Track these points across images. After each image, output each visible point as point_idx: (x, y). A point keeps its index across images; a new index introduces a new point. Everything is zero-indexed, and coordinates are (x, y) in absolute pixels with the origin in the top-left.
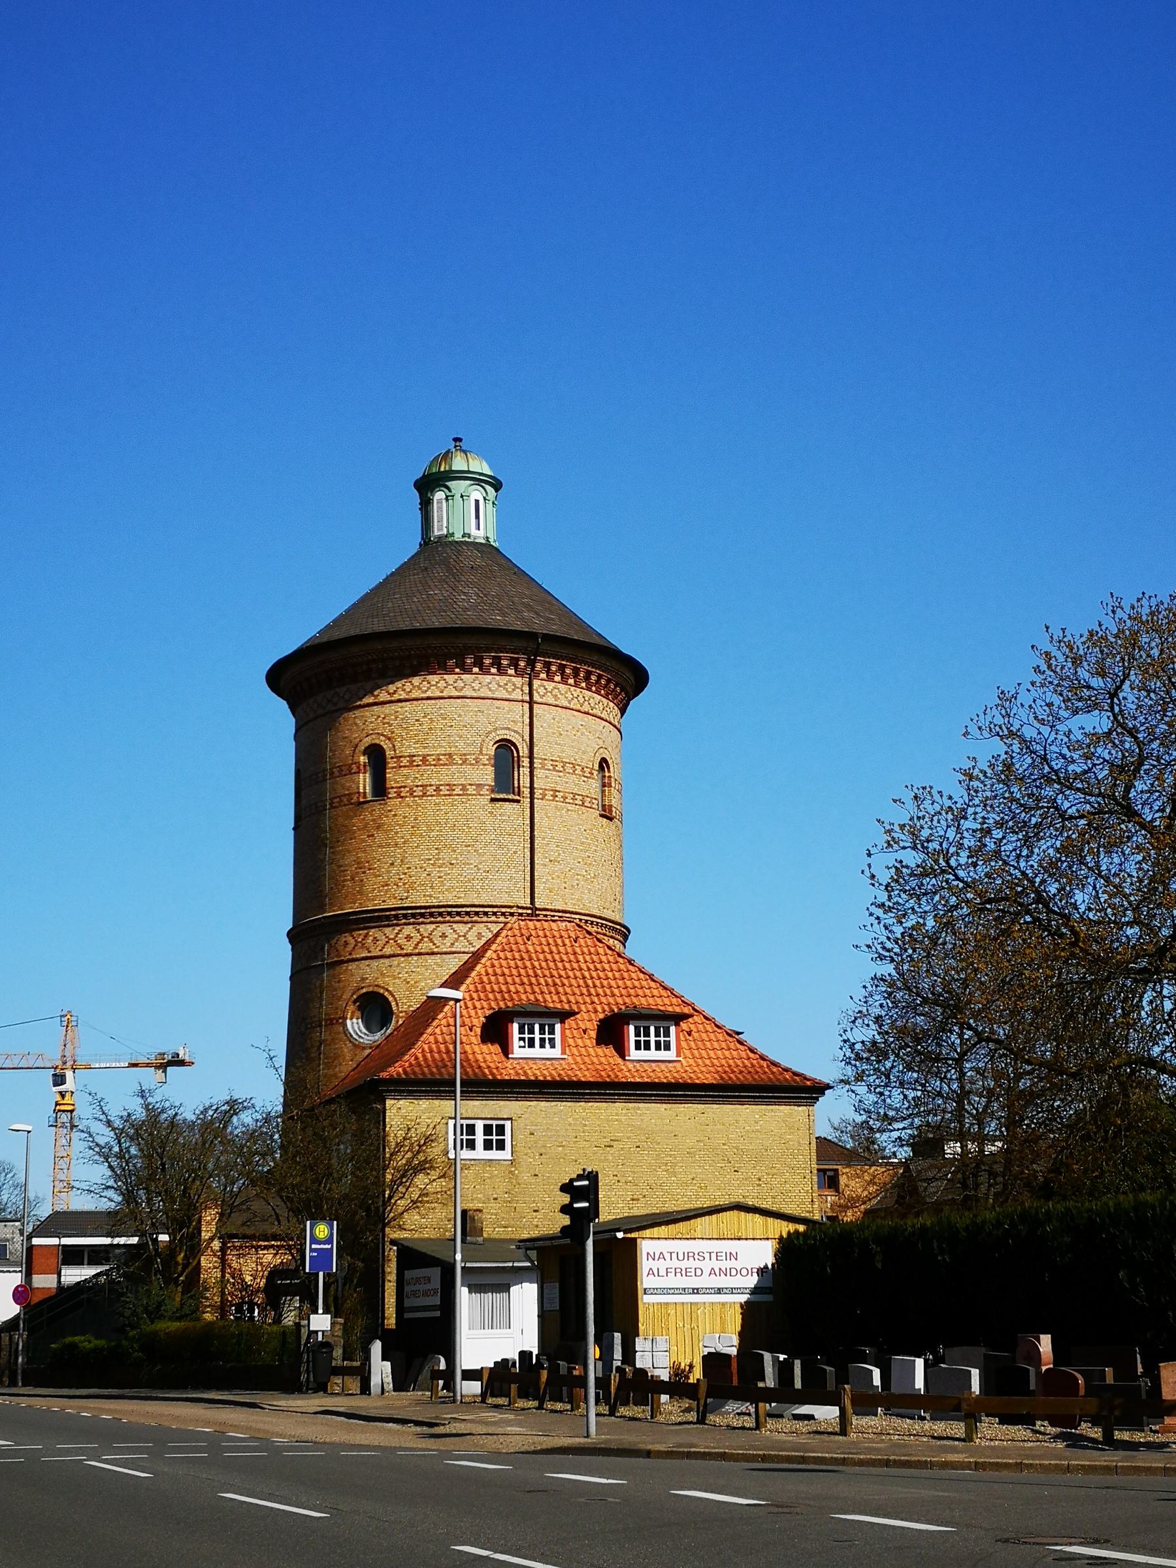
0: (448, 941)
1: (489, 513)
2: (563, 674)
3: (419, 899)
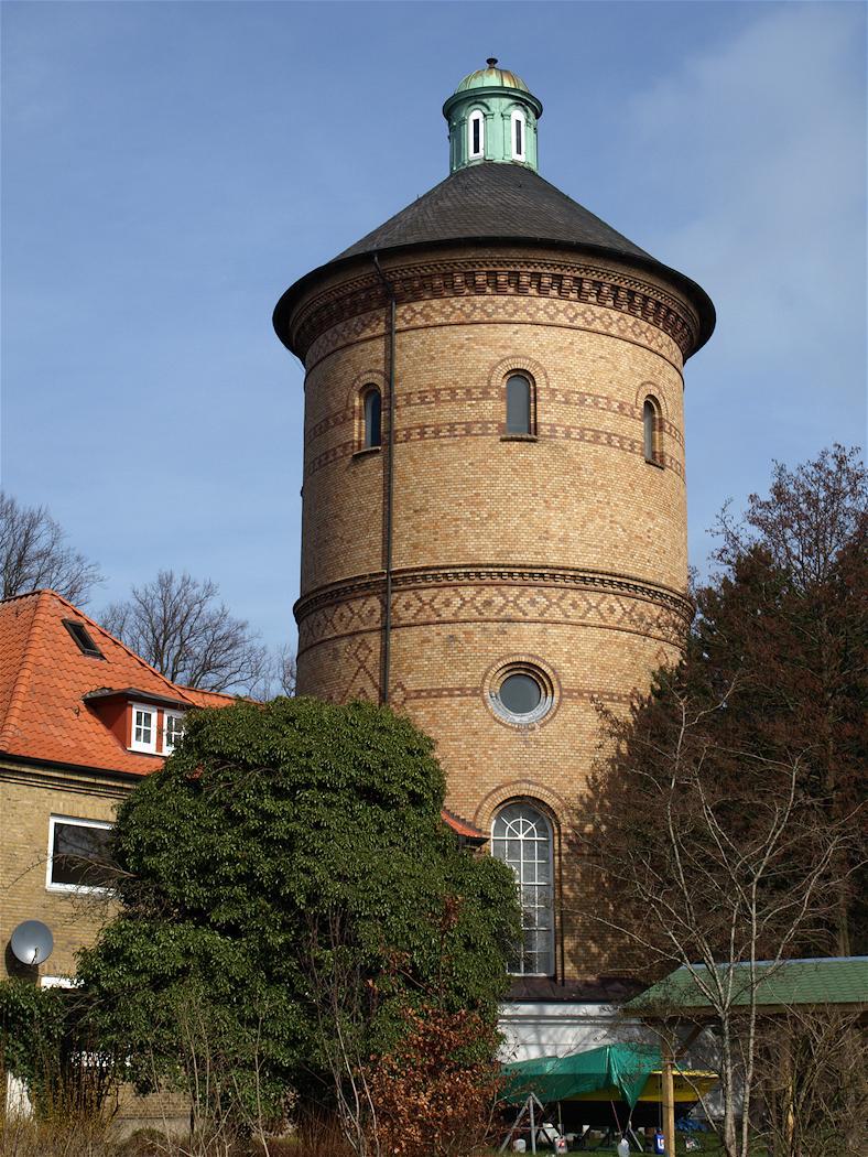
0: (413, 611)
1: (528, 136)
2: (615, 298)
3: (486, 551)
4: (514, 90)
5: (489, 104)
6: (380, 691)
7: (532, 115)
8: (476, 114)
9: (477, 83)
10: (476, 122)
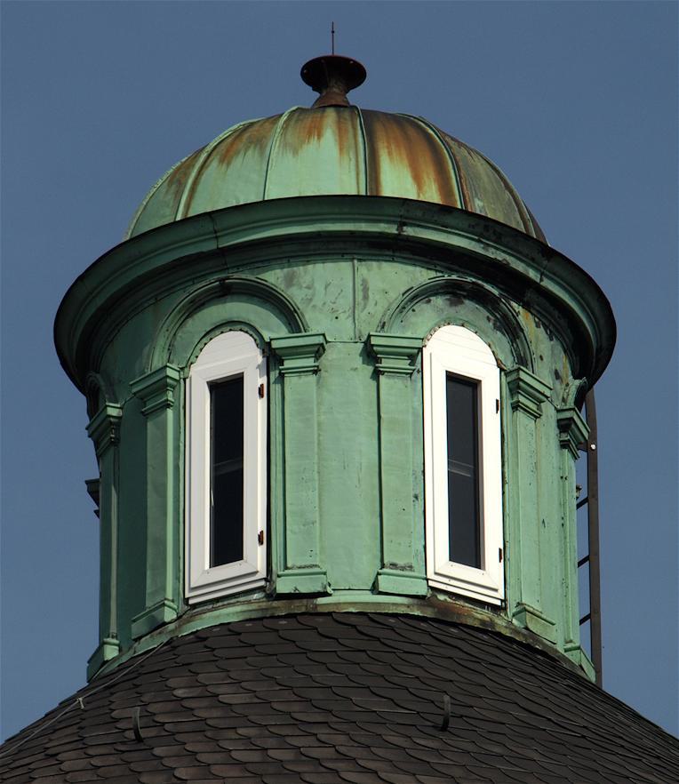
4: (440, 214)
5: (296, 296)
6: (455, 293)
7: (548, 355)
8: (230, 354)
9: (230, 186)
10: (227, 394)
